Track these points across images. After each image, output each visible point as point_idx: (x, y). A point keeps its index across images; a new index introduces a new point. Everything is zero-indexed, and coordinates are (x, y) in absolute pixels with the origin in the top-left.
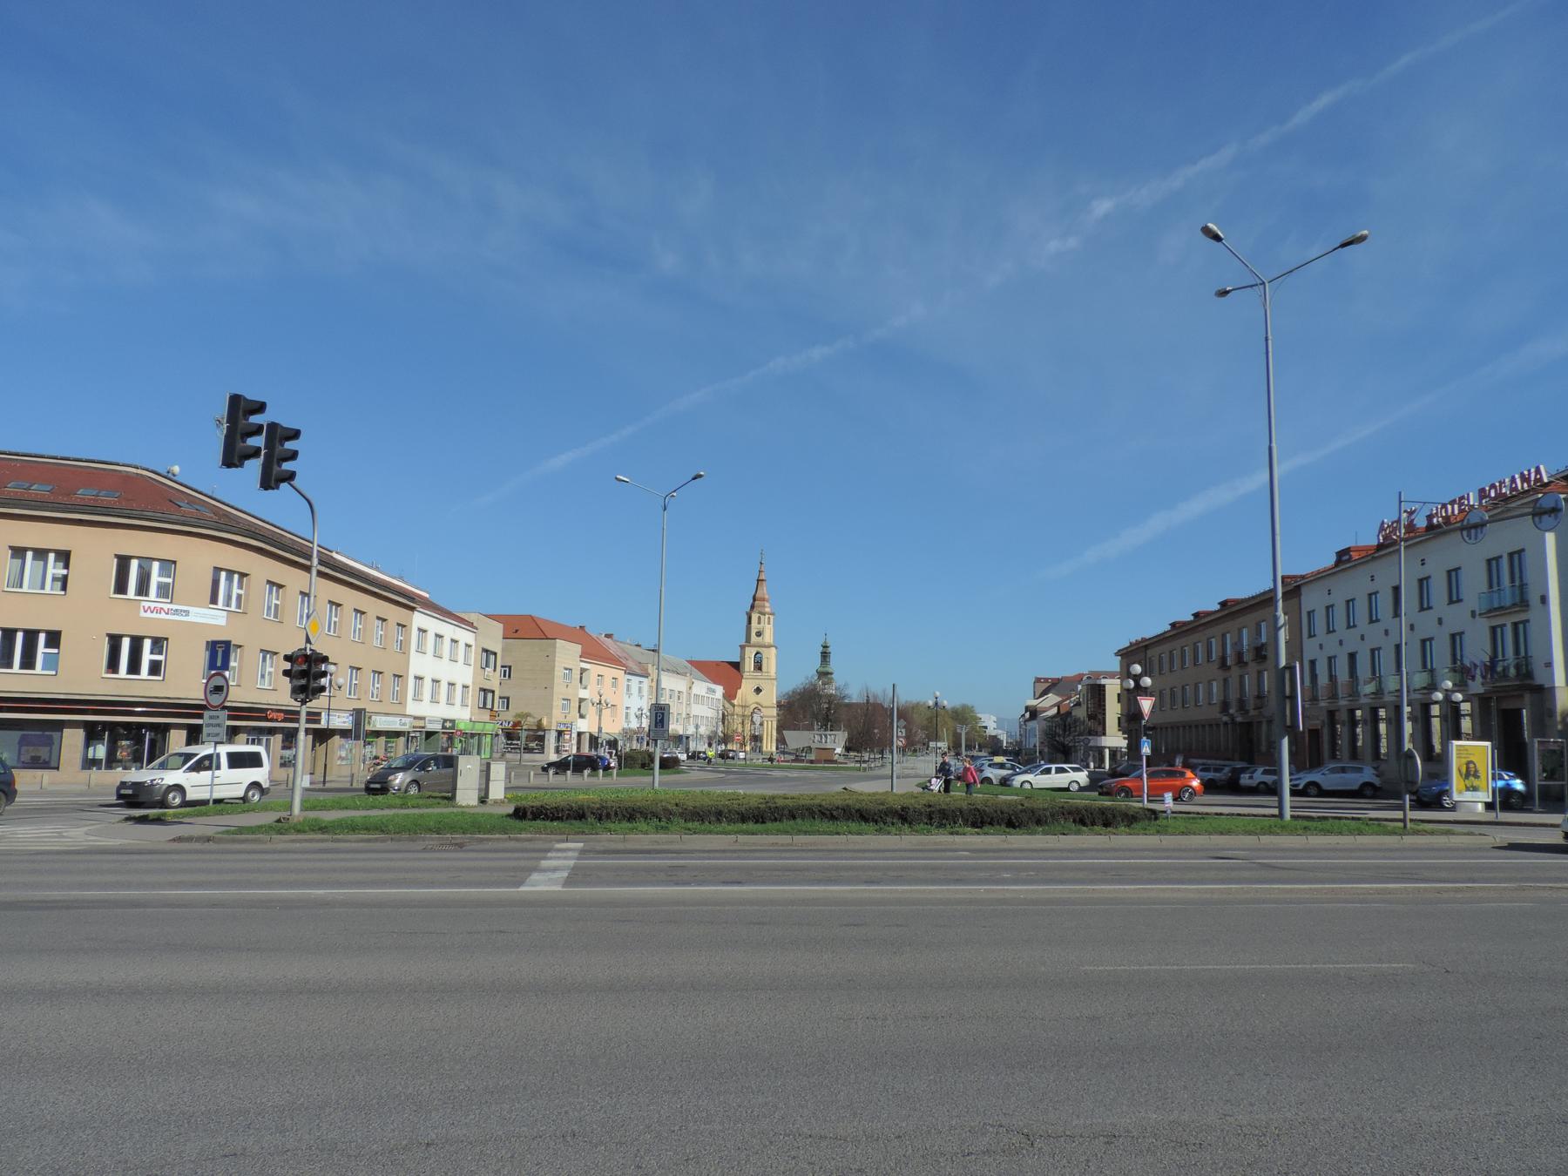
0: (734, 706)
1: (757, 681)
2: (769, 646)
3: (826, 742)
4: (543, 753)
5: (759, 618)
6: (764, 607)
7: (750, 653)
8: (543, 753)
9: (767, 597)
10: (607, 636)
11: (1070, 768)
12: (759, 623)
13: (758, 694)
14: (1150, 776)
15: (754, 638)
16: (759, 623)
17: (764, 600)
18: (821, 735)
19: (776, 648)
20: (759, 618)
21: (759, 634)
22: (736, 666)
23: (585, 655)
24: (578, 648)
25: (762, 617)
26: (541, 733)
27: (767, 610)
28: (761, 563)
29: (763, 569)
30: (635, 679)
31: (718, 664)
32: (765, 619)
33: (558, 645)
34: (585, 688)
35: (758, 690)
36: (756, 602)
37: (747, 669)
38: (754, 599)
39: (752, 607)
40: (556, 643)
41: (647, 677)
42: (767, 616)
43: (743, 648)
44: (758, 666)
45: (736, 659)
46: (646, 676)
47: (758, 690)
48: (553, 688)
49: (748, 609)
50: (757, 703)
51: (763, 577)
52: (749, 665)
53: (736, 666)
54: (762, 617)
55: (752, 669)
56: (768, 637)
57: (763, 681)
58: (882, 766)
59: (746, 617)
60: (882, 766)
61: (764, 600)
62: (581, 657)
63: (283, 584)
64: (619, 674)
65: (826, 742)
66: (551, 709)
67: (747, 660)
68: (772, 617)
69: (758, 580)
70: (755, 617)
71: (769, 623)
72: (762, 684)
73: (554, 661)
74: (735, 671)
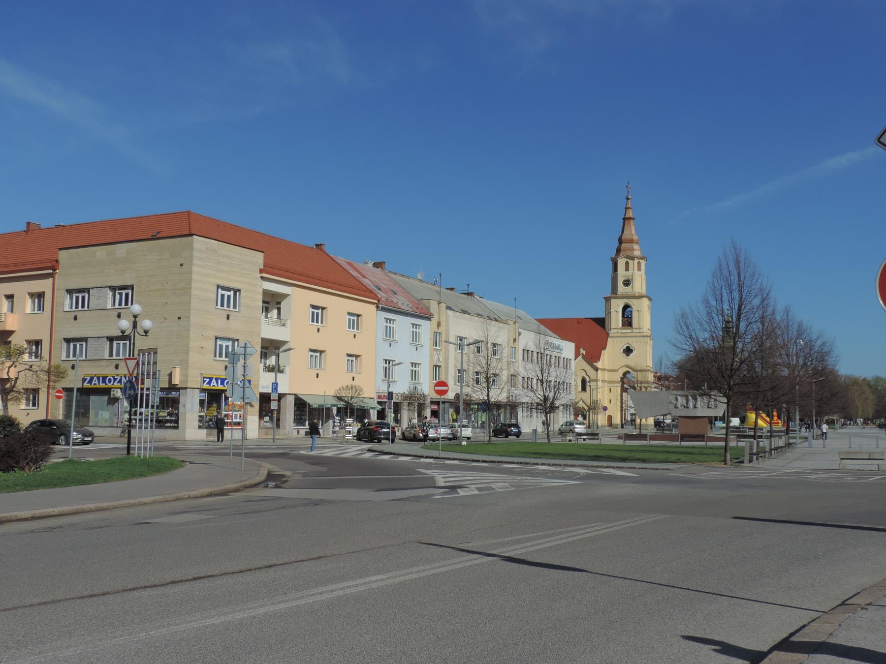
0: (597, 369)
1: (626, 340)
2: (640, 297)
3: (695, 407)
4: (177, 428)
5: (627, 263)
6: (633, 250)
7: (617, 306)
8: (177, 428)
9: (635, 238)
10: (376, 265)
11: (474, 491)
12: (627, 269)
13: (628, 355)
14: (135, 454)
15: (621, 289)
16: (627, 269)
17: (631, 241)
18: (686, 397)
19: (650, 299)
20: (627, 263)
21: (627, 283)
22: (601, 322)
23: (269, 269)
24: (258, 258)
25: (630, 262)
26: (174, 394)
27: (637, 253)
28: (628, 199)
29: (629, 205)
30: (403, 324)
31: (579, 321)
32: (633, 264)
33: (196, 246)
34: (284, 325)
35: (628, 351)
36: (623, 245)
37: (613, 325)
38: (621, 241)
39: (618, 251)
40: (192, 240)
41: (429, 319)
42: (636, 261)
43: (607, 300)
44: (628, 322)
45: (601, 315)
46: (428, 318)
47: (628, 351)
48: (189, 318)
49: (613, 255)
50: (627, 366)
51: (630, 214)
52: (616, 320)
53: (601, 322)
54: (630, 262)
55: (620, 325)
56: (639, 285)
57: (634, 339)
58: (789, 445)
59: (611, 262)
60: (789, 445)
61: (631, 241)
62: (261, 271)
63: (325, 306)
64: (367, 310)
65: (695, 407)
66: (187, 353)
67: (613, 315)
68: (643, 262)
69: (624, 219)
70: (621, 262)
71: (639, 269)
72: (634, 343)
73: (190, 273)
74: (603, 329)
